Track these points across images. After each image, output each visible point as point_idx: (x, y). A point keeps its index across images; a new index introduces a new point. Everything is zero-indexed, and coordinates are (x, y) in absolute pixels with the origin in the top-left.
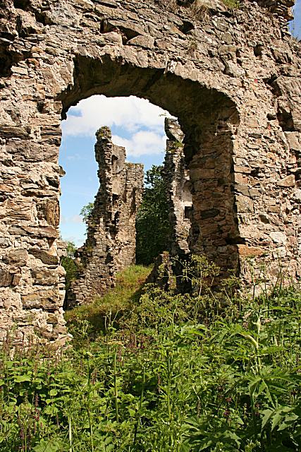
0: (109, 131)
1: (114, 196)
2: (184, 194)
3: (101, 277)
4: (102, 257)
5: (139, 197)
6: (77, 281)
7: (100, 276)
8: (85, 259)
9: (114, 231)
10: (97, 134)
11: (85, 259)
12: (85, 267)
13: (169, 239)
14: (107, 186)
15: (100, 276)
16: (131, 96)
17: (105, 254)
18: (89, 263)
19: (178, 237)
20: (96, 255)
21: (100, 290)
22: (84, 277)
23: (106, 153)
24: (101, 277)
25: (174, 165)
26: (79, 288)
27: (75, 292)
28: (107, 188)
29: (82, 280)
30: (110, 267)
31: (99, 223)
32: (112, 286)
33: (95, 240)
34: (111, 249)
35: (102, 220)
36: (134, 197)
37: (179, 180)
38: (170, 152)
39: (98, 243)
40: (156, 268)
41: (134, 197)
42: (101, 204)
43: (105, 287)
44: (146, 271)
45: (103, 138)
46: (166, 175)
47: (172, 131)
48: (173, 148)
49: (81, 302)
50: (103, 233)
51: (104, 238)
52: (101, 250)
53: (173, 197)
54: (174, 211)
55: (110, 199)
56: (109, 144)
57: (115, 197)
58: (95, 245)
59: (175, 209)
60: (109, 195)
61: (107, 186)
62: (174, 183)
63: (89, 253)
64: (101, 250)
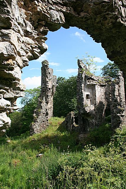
0: (48, 62)
1: (49, 88)
2: (86, 89)
3: (44, 121)
4: (44, 114)
5: (55, 89)
6: (35, 123)
7: (43, 121)
8: (37, 114)
9: (47, 103)
10: (42, 63)
11: (37, 114)
12: (38, 117)
13: (80, 107)
14: (47, 84)
15: (43, 121)
16: (108, 59)
17: (45, 112)
18: (39, 116)
19: (84, 106)
20: (42, 113)
21: (43, 127)
22: (37, 122)
23: (47, 71)
24: (44, 121)
25: (83, 78)
26: (35, 126)
27: (34, 128)
28: (47, 85)
29: (36, 123)
30: (47, 118)
31: (43, 100)
32: (48, 125)
33: (41, 106)
34: (47, 110)
35: (44, 98)
36: (53, 89)
37: (84, 84)
38: (81, 73)
39: (43, 107)
40: (120, 116)
41: (53, 89)
42: (44, 91)
43: (45, 126)
44: (61, 120)
45: (46, 65)
46: (79, 82)
47: (81, 65)
48: (82, 71)
49: (36, 132)
50: (44, 103)
51: (45, 106)
52: (44, 111)
53: (82, 90)
54: (83, 96)
55: (48, 90)
56: (48, 67)
57: (49, 89)
58: (42, 108)
59: (83, 95)
60: (47, 88)
61: (47, 84)
62: (83, 85)
63: (39, 112)
64: (44, 111)
